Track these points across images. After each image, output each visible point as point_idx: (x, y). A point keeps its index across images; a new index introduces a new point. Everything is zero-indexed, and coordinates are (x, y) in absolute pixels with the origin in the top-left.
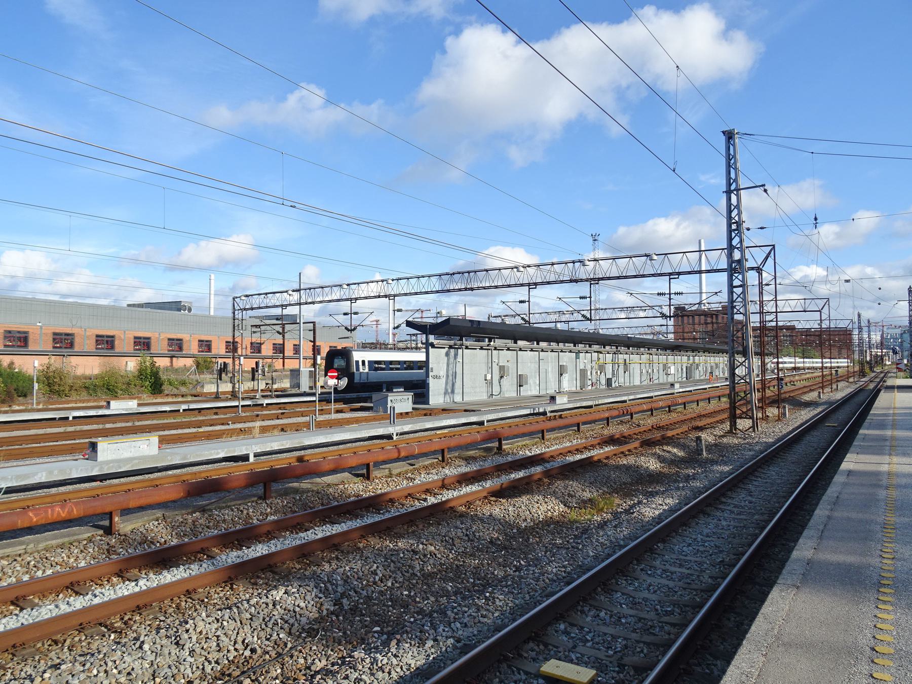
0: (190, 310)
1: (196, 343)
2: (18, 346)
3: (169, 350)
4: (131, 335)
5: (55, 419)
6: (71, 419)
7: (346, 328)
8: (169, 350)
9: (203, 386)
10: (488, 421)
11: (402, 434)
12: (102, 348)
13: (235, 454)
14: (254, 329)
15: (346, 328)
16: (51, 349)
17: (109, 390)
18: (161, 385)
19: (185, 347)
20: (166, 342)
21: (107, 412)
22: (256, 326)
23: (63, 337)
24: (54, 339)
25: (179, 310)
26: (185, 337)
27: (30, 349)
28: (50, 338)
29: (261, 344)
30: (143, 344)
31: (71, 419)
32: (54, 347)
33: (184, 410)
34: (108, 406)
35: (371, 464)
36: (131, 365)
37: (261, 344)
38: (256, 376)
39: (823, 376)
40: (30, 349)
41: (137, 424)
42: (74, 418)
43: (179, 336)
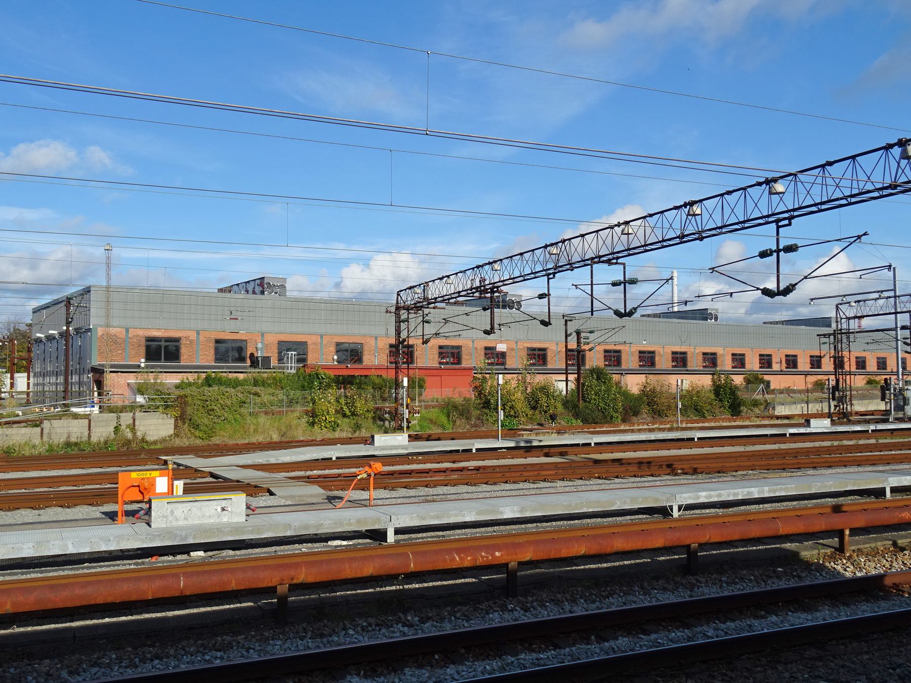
0: (716, 319)
1: (730, 357)
2: (452, 364)
3: (704, 367)
4: (635, 349)
5: (458, 451)
6: (474, 451)
7: (617, 313)
8: (704, 367)
9: (774, 408)
10: (894, 490)
11: (689, 507)
12: (447, 363)
13: (13, 557)
14: (823, 340)
15: (617, 313)
16: (638, 368)
17: (697, 410)
18: (739, 405)
19: (719, 362)
20: (701, 357)
21: (808, 430)
22: (824, 335)
23: (612, 354)
24: (440, 354)
25: (706, 319)
26: (719, 350)
27: (549, 367)
28: (524, 354)
29: (820, 357)
30: (648, 359)
31: (474, 451)
32: (440, 363)
33: (872, 431)
34: (370, 441)
35: (847, 532)
36: (562, 385)
37: (820, 357)
38: (888, 396)
39: (57, 391)
40: (549, 367)
41: (881, 441)
42: (790, 434)
43: (683, 349)
